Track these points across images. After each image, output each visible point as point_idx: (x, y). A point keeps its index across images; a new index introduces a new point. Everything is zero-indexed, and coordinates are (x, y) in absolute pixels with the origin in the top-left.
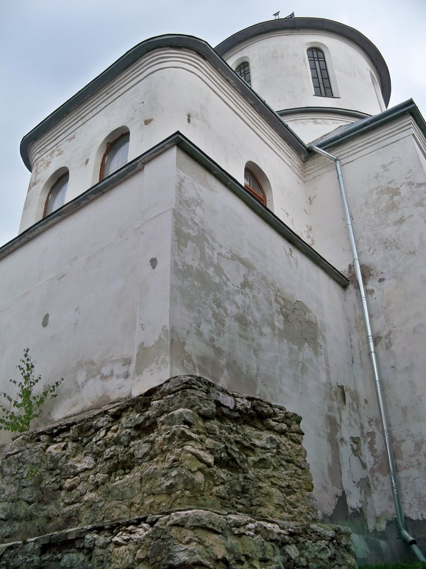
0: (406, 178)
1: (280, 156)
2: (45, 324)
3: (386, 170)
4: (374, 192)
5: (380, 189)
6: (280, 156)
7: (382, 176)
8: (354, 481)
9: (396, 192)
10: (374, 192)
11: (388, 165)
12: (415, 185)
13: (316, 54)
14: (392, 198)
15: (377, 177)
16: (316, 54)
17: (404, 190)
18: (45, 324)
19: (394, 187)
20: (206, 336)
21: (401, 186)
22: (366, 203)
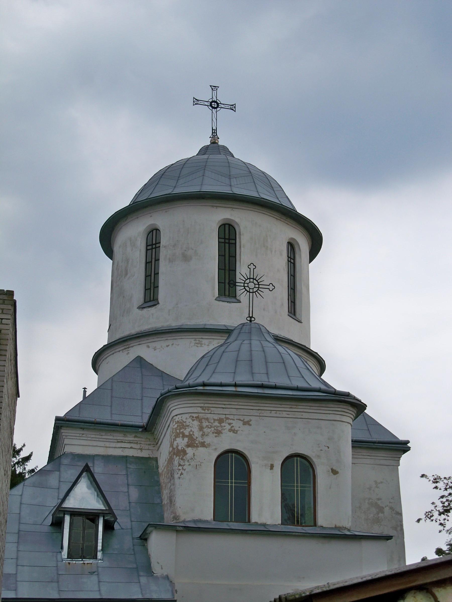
0: (390, 502)
1: (225, 275)
2: (162, 568)
3: (377, 487)
4: (367, 501)
5: (371, 501)
6: (225, 275)
7: (373, 490)
8: (194, 454)
9: (381, 510)
10: (367, 501)
11: (379, 483)
12: (395, 512)
13: (228, 236)
14: (378, 513)
15: (370, 489)
16: (228, 236)
17: (387, 510)
18: (162, 568)
19: (381, 505)
20: (203, 421)
21: (386, 507)
22: (360, 507)
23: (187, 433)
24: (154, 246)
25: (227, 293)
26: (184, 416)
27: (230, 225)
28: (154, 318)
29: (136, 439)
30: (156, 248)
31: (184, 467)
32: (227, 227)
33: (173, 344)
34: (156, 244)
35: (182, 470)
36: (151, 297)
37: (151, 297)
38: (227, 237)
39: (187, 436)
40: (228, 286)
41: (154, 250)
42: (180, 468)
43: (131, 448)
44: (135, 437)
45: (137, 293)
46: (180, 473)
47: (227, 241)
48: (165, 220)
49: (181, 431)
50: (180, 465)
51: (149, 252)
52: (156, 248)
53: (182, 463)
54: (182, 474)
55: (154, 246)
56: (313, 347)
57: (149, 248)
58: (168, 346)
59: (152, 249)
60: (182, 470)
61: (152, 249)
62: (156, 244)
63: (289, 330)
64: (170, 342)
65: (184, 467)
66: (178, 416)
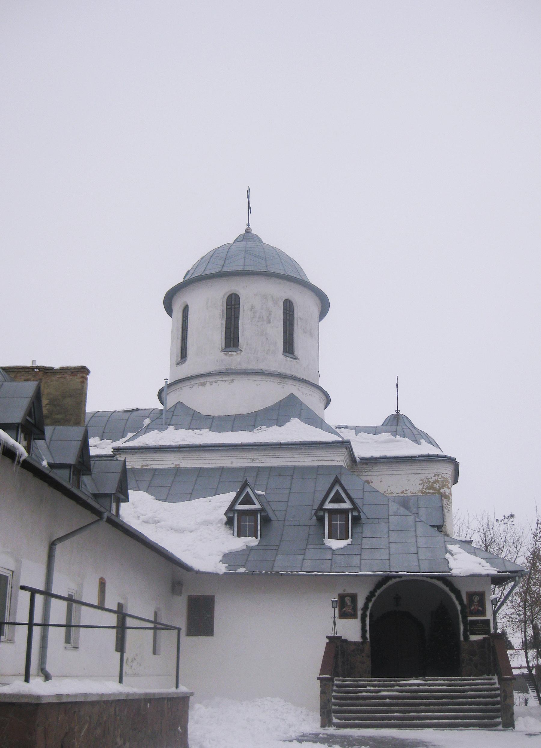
28: (236, 360)
30: (235, 308)
36: (231, 340)
37: (231, 340)
40: (289, 347)
48: (250, 293)
62: (235, 305)
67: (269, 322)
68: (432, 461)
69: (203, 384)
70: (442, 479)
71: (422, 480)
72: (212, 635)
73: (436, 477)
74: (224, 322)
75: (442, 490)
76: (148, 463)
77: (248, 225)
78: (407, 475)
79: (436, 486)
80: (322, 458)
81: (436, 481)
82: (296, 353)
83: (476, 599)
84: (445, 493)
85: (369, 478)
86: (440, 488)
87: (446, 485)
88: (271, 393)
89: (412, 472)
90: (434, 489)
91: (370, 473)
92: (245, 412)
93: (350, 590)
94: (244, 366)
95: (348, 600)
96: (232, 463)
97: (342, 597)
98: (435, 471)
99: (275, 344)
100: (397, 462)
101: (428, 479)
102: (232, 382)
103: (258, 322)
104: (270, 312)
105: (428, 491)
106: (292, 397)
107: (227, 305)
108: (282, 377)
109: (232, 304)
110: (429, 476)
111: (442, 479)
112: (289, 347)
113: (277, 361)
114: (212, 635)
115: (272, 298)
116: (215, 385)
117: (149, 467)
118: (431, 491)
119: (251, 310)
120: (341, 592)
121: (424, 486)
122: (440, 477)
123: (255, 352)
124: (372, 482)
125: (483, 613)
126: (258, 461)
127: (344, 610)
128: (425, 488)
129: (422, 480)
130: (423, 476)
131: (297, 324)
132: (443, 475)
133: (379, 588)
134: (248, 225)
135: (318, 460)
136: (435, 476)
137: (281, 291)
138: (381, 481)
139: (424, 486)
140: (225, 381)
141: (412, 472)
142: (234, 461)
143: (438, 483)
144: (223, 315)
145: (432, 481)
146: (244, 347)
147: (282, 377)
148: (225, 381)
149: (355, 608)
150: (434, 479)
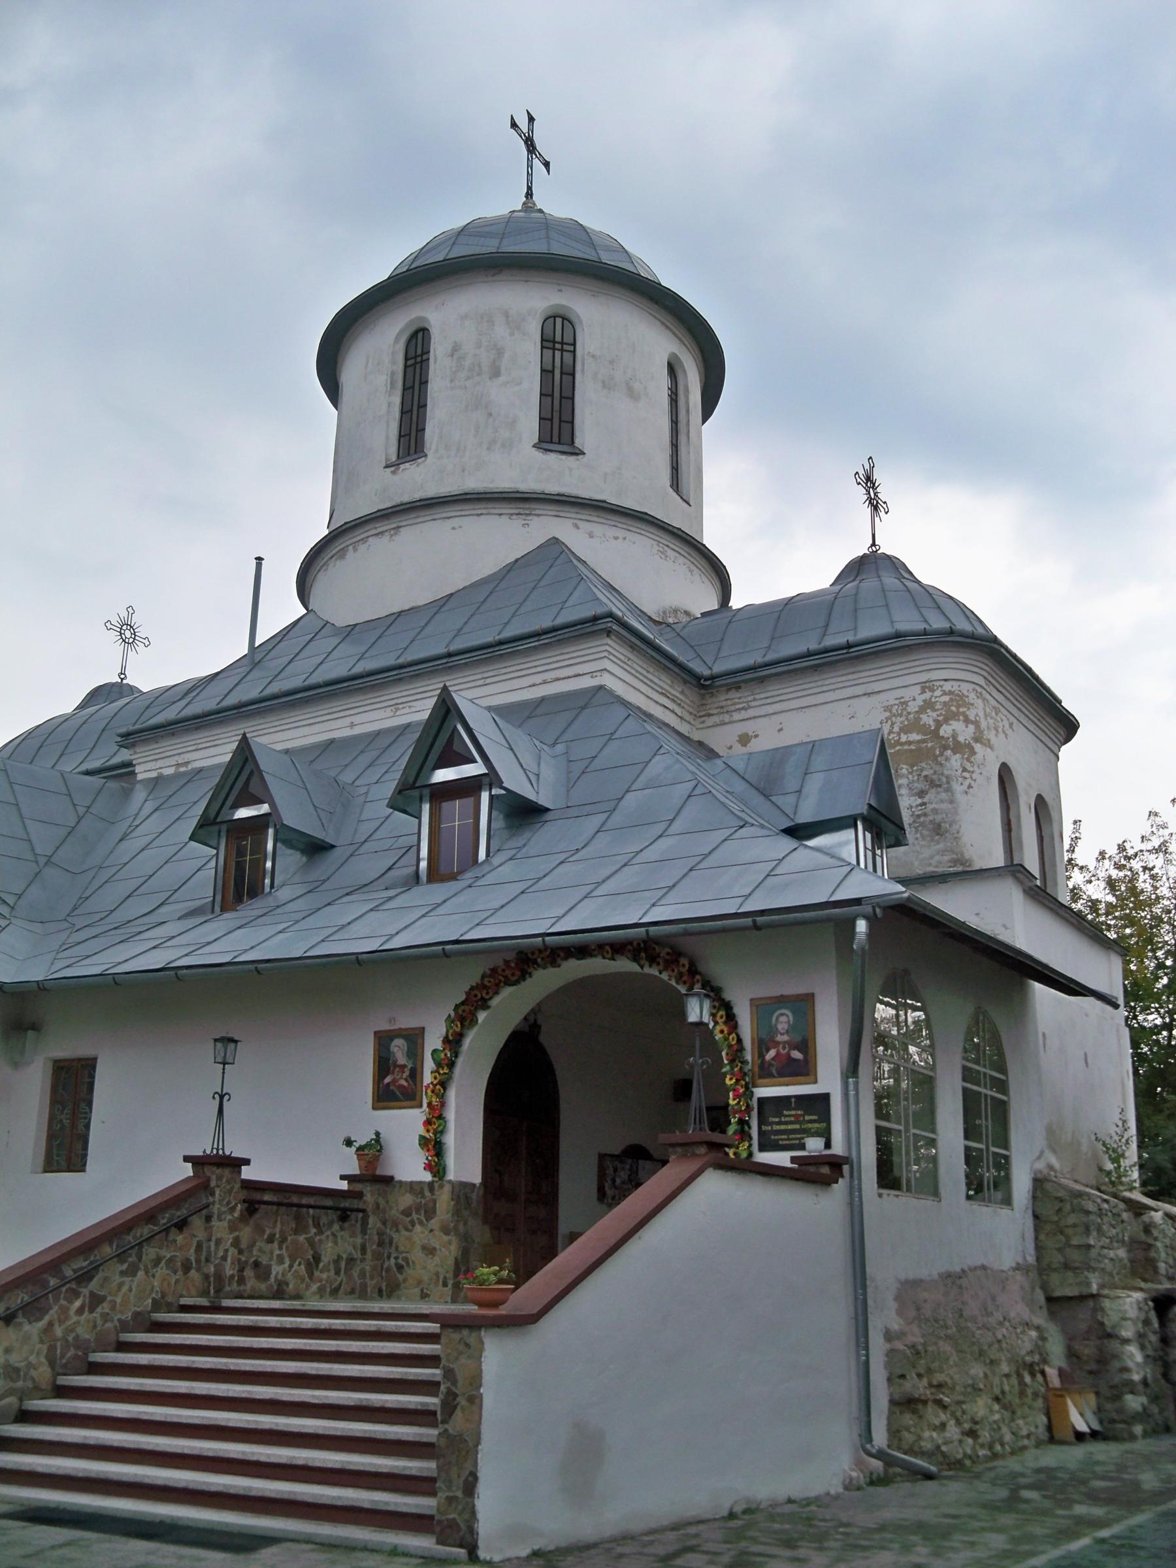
23: (972, 718)
24: (419, 359)
25: (555, 439)
26: (965, 687)
27: (564, 319)
28: (419, 479)
29: (681, 697)
30: (422, 361)
31: (974, 776)
32: (559, 321)
33: (625, 538)
34: (421, 356)
35: (969, 780)
36: (411, 441)
37: (411, 441)
38: (558, 338)
39: (972, 723)
40: (558, 428)
41: (418, 366)
42: (966, 774)
43: (673, 711)
44: (682, 692)
45: (384, 434)
46: (967, 783)
47: (558, 346)
48: (449, 316)
49: (961, 710)
50: (965, 770)
51: (410, 370)
52: (422, 361)
53: (968, 766)
54: (970, 787)
55: (419, 359)
56: (711, 540)
57: (409, 363)
58: (616, 538)
59: (416, 363)
60: (969, 780)
61: (416, 363)
62: (421, 356)
63: (671, 512)
64: (621, 533)
65: (974, 776)
66: (951, 683)
67: (496, 373)
68: (910, 648)
69: (342, 554)
70: (946, 698)
71: (888, 709)
72: (84, 1171)
73: (928, 695)
74: (397, 400)
75: (946, 731)
76: (187, 757)
77: (529, 194)
78: (848, 702)
79: (928, 719)
80: (553, 675)
81: (928, 705)
82: (578, 442)
83: (783, 1020)
84: (954, 736)
85: (749, 727)
86: (939, 724)
87: (964, 714)
88: (501, 541)
89: (859, 690)
90: (923, 729)
91: (751, 713)
92: (421, 603)
93: (407, 1022)
94: (431, 491)
95: (399, 1049)
96: (352, 725)
97: (383, 1040)
98: (923, 677)
99: (512, 424)
100: (815, 668)
101: (906, 703)
102: (396, 534)
103: (468, 378)
104: (500, 352)
105: (904, 738)
106: (555, 541)
107: (406, 359)
108: (521, 501)
109: (417, 349)
110: (907, 694)
111: (946, 698)
112: (558, 428)
113: (526, 466)
114: (84, 1171)
115: (506, 315)
116: (362, 548)
117: (190, 767)
118: (915, 737)
119: (452, 355)
120: (384, 1026)
121: (893, 724)
122: (938, 693)
123: (458, 449)
124: (756, 736)
125: (804, 1069)
126: (407, 710)
127: (388, 1080)
128: (896, 729)
129: (888, 709)
130: (890, 698)
131: (583, 370)
132: (947, 686)
133: (484, 1004)
134: (529, 194)
135: (545, 682)
136: (923, 692)
137: (531, 300)
138: (781, 730)
139: (893, 724)
140: (382, 533)
141: (859, 690)
142: (357, 719)
143: (934, 710)
144: (393, 384)
145: (913, 707)
146: (434, 447)
147: (521, 501)
148: (382, 533)
149: (415, 1074)
150: (920, 701)
